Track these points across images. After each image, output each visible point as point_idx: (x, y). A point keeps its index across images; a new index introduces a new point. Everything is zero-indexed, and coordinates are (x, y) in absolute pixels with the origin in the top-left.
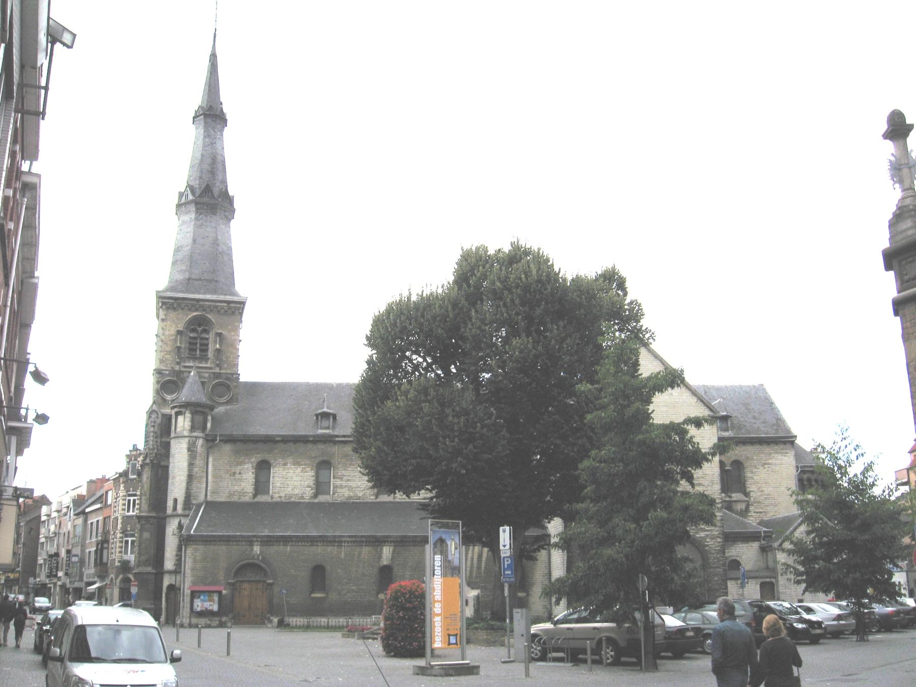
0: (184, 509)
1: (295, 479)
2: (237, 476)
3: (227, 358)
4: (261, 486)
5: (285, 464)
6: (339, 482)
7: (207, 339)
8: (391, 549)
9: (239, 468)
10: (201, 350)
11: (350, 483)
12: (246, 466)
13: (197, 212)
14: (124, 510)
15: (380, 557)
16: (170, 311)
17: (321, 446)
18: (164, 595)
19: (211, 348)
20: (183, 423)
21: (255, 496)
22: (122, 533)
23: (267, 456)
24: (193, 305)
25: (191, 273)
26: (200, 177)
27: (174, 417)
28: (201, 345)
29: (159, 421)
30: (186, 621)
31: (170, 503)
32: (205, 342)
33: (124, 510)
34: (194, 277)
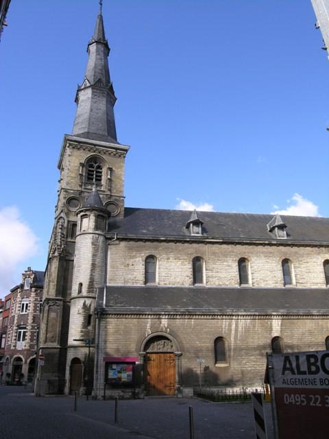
0: (89, 292)
1: (176, 270)
2: (131, 267)
3: (116, 185)
4: (149, 275)
5: (168, 259)
6: (210, 274)
7: (101, 172)
8: (280, 322)
9: (132, 260)
10: (96, 180)
11: (219, 275)
12: (137, 259)
13: (92, 94)
14: (19, 310)
15: (271, 329)
16: (75, 150)
17: (195, 245)
18: (68, 368)
19: (104, 179)
20: (88, 223)
21: (146, 282)
22: (17, 326)
23: (153, 252)
24: (92, 148)
25: (89, 129)
26: (94, 75)
27: (79, 223)
28: (96, 176)
29: (65, 225)
30: (100, 393)
31: (75, 288)
32: (99, 174)
33: (19, 310)
34: (91, 131)
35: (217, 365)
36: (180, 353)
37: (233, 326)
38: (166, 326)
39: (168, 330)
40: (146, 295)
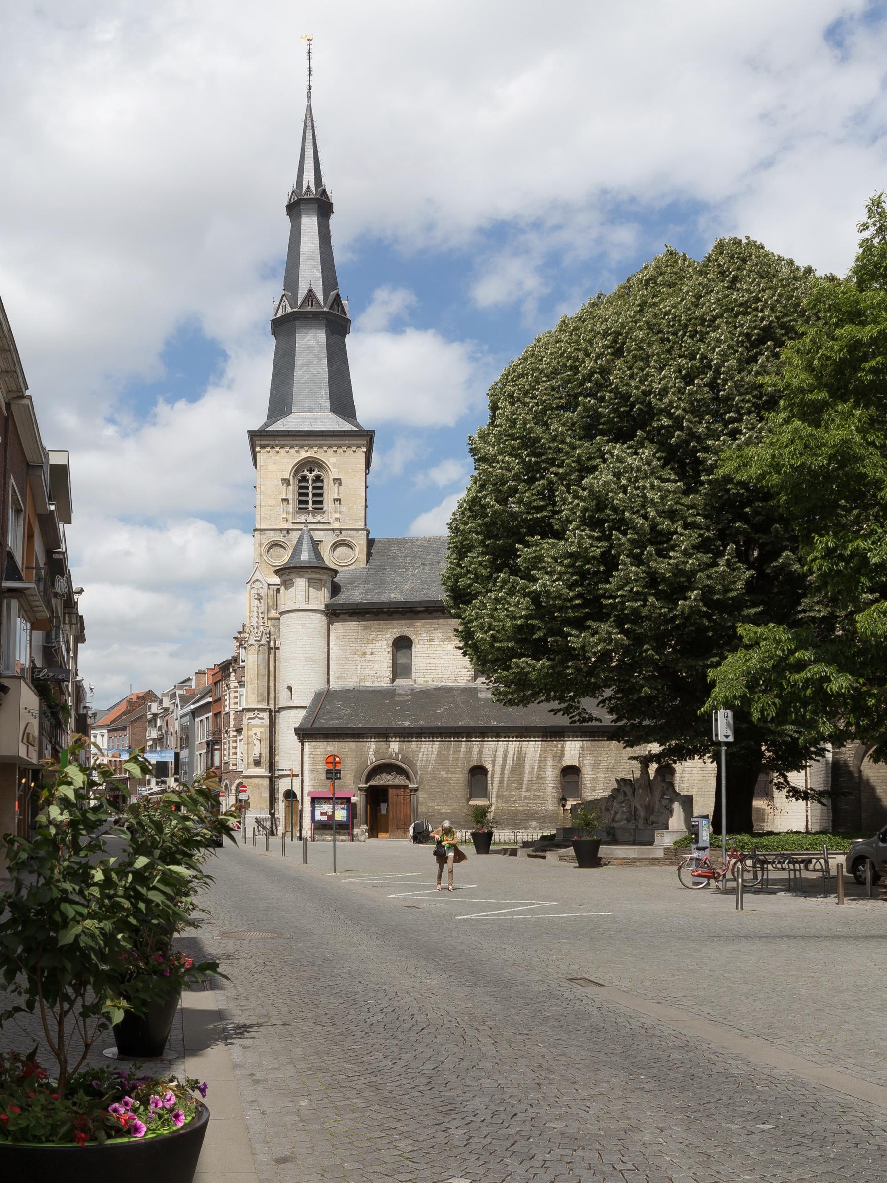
2: (369, 657)
5: (431, 640)
9: (370, 646)
21: (393, 680)
35: (471, 803)
36: (416, 786)
37: (500, 753)
38: (397, 751)
39: (400, 756)
40: (141, 861)
